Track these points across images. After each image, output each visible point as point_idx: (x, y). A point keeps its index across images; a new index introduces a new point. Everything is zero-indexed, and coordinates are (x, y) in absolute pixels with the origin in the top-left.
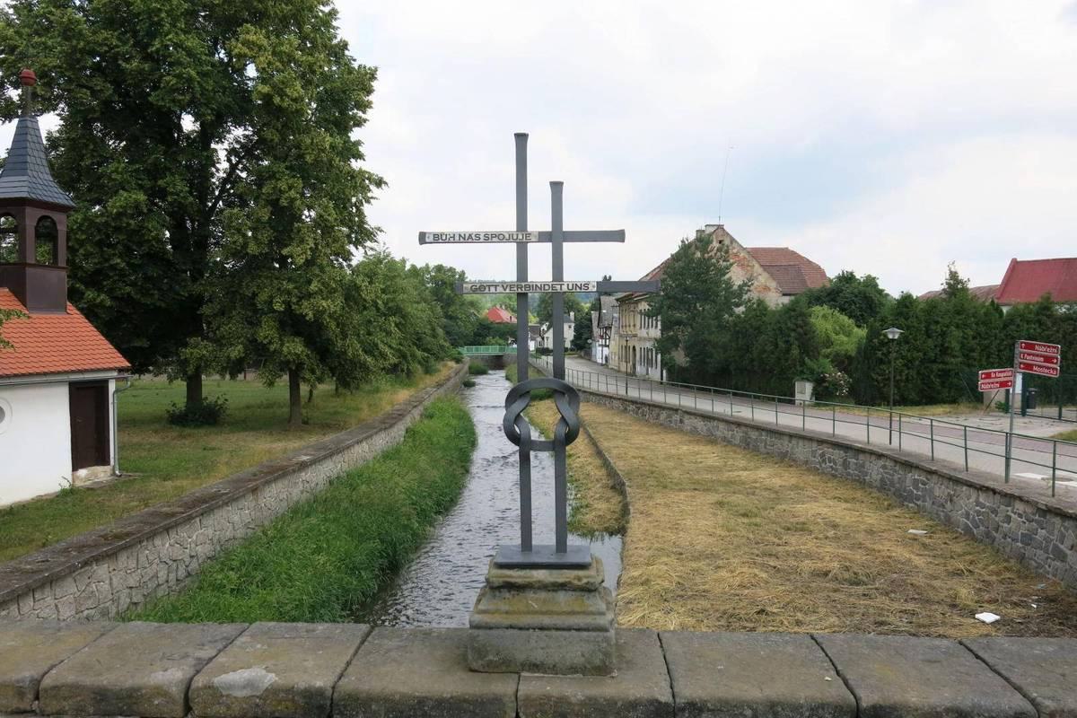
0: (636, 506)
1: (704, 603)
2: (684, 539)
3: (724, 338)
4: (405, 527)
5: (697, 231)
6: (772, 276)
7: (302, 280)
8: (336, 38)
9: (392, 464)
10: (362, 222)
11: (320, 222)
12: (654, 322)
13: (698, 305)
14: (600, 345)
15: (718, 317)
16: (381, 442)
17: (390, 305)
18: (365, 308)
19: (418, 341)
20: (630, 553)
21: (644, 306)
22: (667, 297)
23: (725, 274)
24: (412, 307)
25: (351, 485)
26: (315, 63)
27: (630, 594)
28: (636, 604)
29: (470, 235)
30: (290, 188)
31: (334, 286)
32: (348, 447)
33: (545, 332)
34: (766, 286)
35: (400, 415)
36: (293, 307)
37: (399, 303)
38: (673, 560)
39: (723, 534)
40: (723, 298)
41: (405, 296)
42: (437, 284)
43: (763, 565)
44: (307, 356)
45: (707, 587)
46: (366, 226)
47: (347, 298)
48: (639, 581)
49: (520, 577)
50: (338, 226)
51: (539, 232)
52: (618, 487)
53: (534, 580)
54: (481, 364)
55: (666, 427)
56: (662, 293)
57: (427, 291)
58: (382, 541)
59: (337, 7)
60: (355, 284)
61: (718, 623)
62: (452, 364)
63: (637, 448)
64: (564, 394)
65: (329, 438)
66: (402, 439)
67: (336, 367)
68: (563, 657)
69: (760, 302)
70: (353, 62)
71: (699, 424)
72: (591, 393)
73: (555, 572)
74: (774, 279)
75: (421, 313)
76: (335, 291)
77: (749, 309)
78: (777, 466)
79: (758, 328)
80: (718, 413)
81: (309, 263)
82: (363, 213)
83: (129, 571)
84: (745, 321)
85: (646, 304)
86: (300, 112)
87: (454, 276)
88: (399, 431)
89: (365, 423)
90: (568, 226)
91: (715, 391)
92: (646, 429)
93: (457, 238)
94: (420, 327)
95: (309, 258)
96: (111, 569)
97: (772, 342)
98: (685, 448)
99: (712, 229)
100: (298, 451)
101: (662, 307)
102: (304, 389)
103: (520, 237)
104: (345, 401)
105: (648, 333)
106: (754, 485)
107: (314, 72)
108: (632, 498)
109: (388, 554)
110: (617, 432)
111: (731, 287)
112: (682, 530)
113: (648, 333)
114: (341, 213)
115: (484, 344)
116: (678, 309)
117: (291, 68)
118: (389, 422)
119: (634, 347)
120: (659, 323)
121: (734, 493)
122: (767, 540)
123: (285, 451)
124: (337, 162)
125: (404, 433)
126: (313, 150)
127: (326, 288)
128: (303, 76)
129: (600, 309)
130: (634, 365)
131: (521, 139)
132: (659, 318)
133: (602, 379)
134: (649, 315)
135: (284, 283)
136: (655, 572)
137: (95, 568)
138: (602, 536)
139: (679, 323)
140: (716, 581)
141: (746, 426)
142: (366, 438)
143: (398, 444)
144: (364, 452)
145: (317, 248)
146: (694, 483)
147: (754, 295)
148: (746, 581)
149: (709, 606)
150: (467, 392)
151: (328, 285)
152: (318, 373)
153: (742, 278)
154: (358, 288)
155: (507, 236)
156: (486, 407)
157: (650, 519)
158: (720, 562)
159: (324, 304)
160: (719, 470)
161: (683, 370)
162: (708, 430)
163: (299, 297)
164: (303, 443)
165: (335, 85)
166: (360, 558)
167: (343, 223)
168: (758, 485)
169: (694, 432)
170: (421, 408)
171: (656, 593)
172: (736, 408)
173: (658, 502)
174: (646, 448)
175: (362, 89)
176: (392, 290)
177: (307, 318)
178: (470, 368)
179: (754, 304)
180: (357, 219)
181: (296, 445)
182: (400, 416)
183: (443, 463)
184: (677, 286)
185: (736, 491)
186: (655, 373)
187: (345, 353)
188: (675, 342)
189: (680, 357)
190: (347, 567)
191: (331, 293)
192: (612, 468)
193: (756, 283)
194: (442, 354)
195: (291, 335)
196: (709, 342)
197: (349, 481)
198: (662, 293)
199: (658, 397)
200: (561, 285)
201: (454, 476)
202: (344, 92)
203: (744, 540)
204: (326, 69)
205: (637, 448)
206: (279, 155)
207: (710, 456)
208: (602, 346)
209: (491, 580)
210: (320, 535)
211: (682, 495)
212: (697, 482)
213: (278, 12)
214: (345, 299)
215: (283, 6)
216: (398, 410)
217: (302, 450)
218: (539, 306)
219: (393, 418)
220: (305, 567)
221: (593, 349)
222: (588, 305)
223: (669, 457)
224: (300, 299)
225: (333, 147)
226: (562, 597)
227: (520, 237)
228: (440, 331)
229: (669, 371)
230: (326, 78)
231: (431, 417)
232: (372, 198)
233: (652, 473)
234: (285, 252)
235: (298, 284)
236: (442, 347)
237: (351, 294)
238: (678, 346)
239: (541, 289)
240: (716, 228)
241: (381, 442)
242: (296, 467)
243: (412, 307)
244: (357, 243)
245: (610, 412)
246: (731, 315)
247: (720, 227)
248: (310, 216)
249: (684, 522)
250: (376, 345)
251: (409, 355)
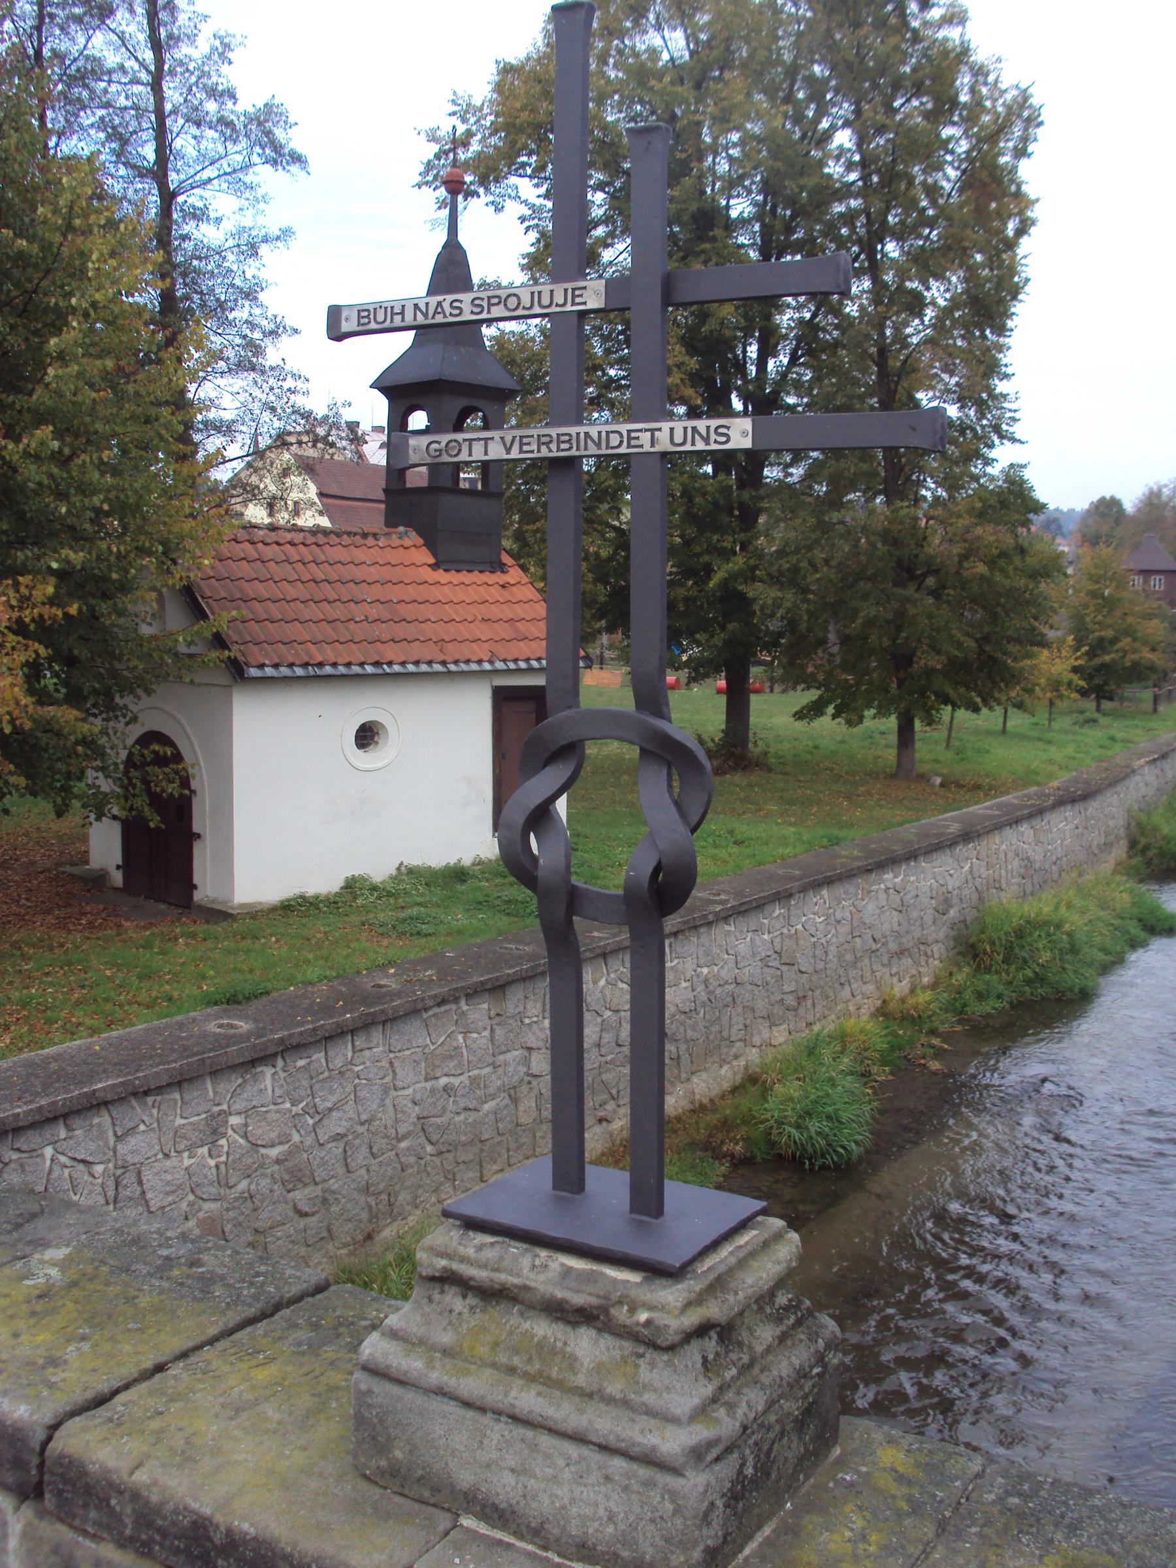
68: (563, 1508)
83: (527, 1021)
96: (493, 1013)
137: (465, 1008)
200: (652, 431)
226: (586, 1345)
239: (598, 445)
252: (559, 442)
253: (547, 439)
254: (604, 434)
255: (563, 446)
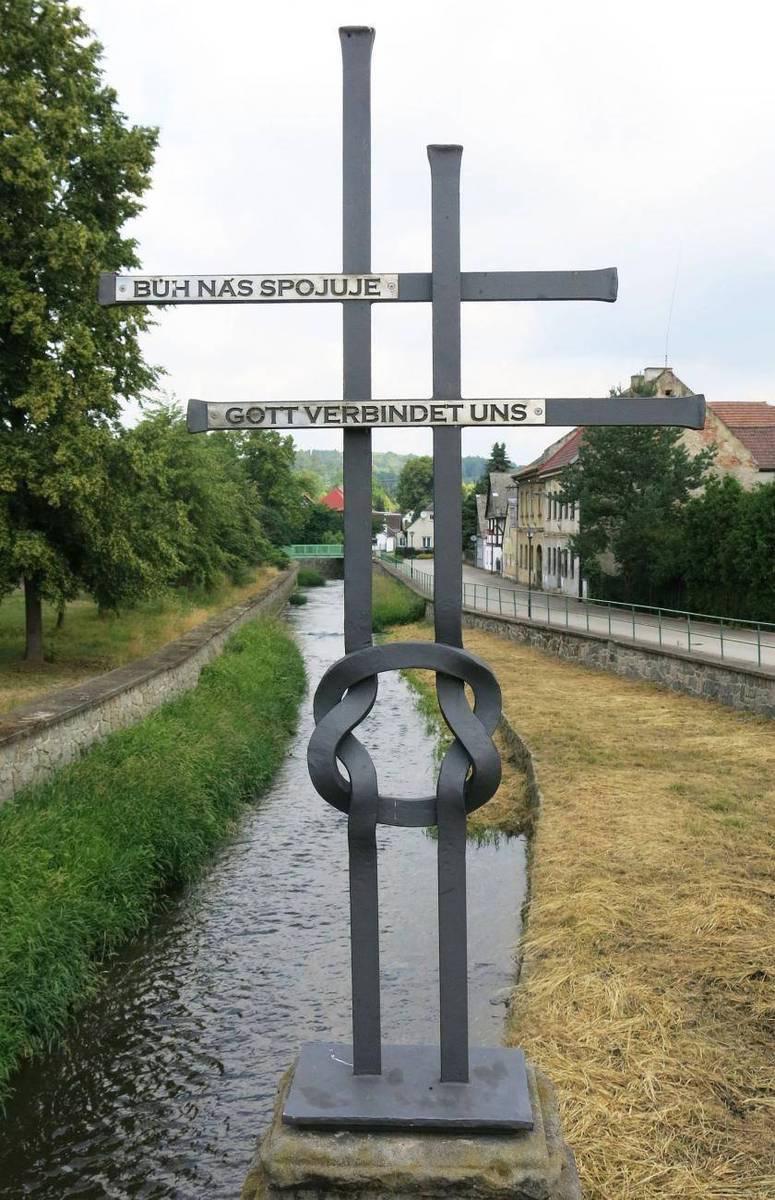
0: (549, 793)
1: (663, 959)
2: (625, 846)
3: (675, 535)
4: (194, 825)
5: (633, 377)
6: (746, 444)
7: (43, 446)
8: (99, 84)
9: (176, 725)
10: (136, 359)
11: (72, 358)
12: (570, 510)
13: (635, 485)
14: (488, 544)
15: (665, 503)
16: (163, 688)
17: (182, 484)
18: (139, 488)
19: (223, 538)
20: (543, 869)
21: (554, 487)
22: (589, 473)
23: (674, 440)
24: (214, 487)
25: (112, 758)
26: (66, 120)
27: (544, 940)
28: (554, 960)
29: (227, 283)
30: (27, 307)
31: (91, 454)
32: (111, 698)
33: (409, 525)
34: (734, 458)
35: (192, 648)
36: (31, 486)
37: (195, 481)
38: (609, 883)
39: (686, 838)
40: (672, 475)
41: (204, 471)
42: (252, 454)
43: (753, 892)
44: (51, 559)
45: (665, 930)
46: (140, 365)
47: (113, 472)
48: (558, 918)
49: (348, 1161)
50: (98, 364)
51: (401, 276)
52: (520, 760)
53: (386, 1171)
54: (315, 571)
55: (590, 667)
56: (582, 468)
57: (237, 466)
58: (158, 847)
59: (102, 40)
60: (124, 452)
61: (688, 995)
62: (273, 571)
63: (547, 699)
64: (460, 682)
65: (84, 683)
66: (195, 684)
67: (94, 577)
69: (729, 481)
70: (122, 120)
71: (640, 663)
72: (477, 616)
73: (440, 1145)
74: (746, 447)
75: (227, 496)
76: (93, 461)
77: (711, 491)
78: (761, 728)
79: (725, 520)
80: (669, 647)
81: (56, 420)
82: (136, 345)
84: (706, 509)
85: (557, 484)
86: (43, 194)
87: (276, 443)
88: (190, 672)
89: (137, 660)
90: (473, 259)
91: (664, 614)
92: (558, 670)
93: (194, 294)
94: (226, 517)
95: (54, 412)
97: (746, 540)
98: (619, 699)
99: (656, 374)
100: (34, 705)
101: (580, 489)
102: (48, 610)
103: (353, 287)
104: (111, 626)
105: (560, 528)
106: (727, 758)
107: (63, 135)
108: (542, 778)
109: (166, 866)
110: (516, 674)
111: (685, 458)
112: (622, 832)
113: (560, 528)
114: (104, 345)
115: (320, 542)
116: (605, 491)
117: (31, 129)
118: (174, 659)
119: (539, 548)
120: (577, 512)
121: (698, 771)
122: (757, 851)
123: (13, 703)
124: (98, 269)
125: (197, 675)
126: (61, 250)
127: (81, 458)
128: (47, 140)
129: (489, 493)
130: (539, 574)
131: (357, 41)
132: (577, 504)
133: (494, 594)
134: (562, 500)
135: (17, 450)
136: (583, 903)
138: (497, 838)
139: (607, 511)
140: (679, 919)
141: (713, 666)
142: (140, 684)
143: (187, 692)
144: (134, 705)
145: (66, 397)
146: (635, 755)
147: (719, 471)
148: (729, 919)
149: (672, 964)
150: (298, 613)
151: (83, 453)
152: (67, 585)
153: (700, 447)
154: (126, 458)
155: (319, 287)
156: (324, 635)
157: (570, 814)
158: (684, 887)
159: (76, 482)
160: (674, 734)
161: (611, 581)
162: (653, 672)
163: (39, 471)
164: (43, 691)
165: (96, 153)
166: (121, 874)
167: (106, 360)
168: (733, 759)
169: (632, 674)
170: (225, 637)
171: (586, 939)
172: (695, 639)
173: (583, 785)
174: (561, 699)
175: (136, 160)
176: (184, 462)
177: (50, 503)
178: (300, 576)
179: (719, 483)
180: (128, 355)
181: (31, 695)
182: (193, 650)
183: (255, 720)
184: (603, 457)
185: (702, 768)
186: (571, 586)
187: (108, 555)
188: (601, 541)
189: (609, 563)
190: (101, 888)
191: (86, 466)
192: (510, 731)
193: (721, 453)
194: (258, 556)
195: (28, 528)
196: (652, 539)
197: (111, 751)
198: (582, 468)
199: (577, 622)
200: (455, 407)
201: (271, 742)
202: (110, 165)
203: (720, 850)
204: (84, 131)
205: (547, 699)
206: (10, 258)
207: (658, 712)
208: (492, 545)
209: (275, 1167)
210: (61, 838)
211: (619, 774)
212: (642, 754)
213: (12, 45)
214: (110, 475)
215: (20, 36)
216: (190, 640)
217: (39, 702)
218: (400, 487)
219: (182, 653)
220: (34, 889)
221: (479, 550)
222: (472, 486)
223: (596, 713)
224: (41, 473)
225: (91, 246)
227: (353, 287)
228: (256, 523)
229: (592, 585)
230: (83, 144)
231: (239, 649)
232: (150, 323)
233: (572, 738)
234: (18, 402)
235: (38, 452)
236: (258, 546)
237: (117, 463)
238: (604, 546)
240: (660, 372)
241: (163, 688)
242: (27, 731)
243: (214, 487)
244: (128, 391)
245: (506, 643)
246: (684, 500)
247: (667, 371)
248: (56, 349)
249: (624, 819)
250: (155, 544)
251: (208, 558)
252: (365, 414)
253: (353, 411)
254: (408, 408)
255: (368, 417)
